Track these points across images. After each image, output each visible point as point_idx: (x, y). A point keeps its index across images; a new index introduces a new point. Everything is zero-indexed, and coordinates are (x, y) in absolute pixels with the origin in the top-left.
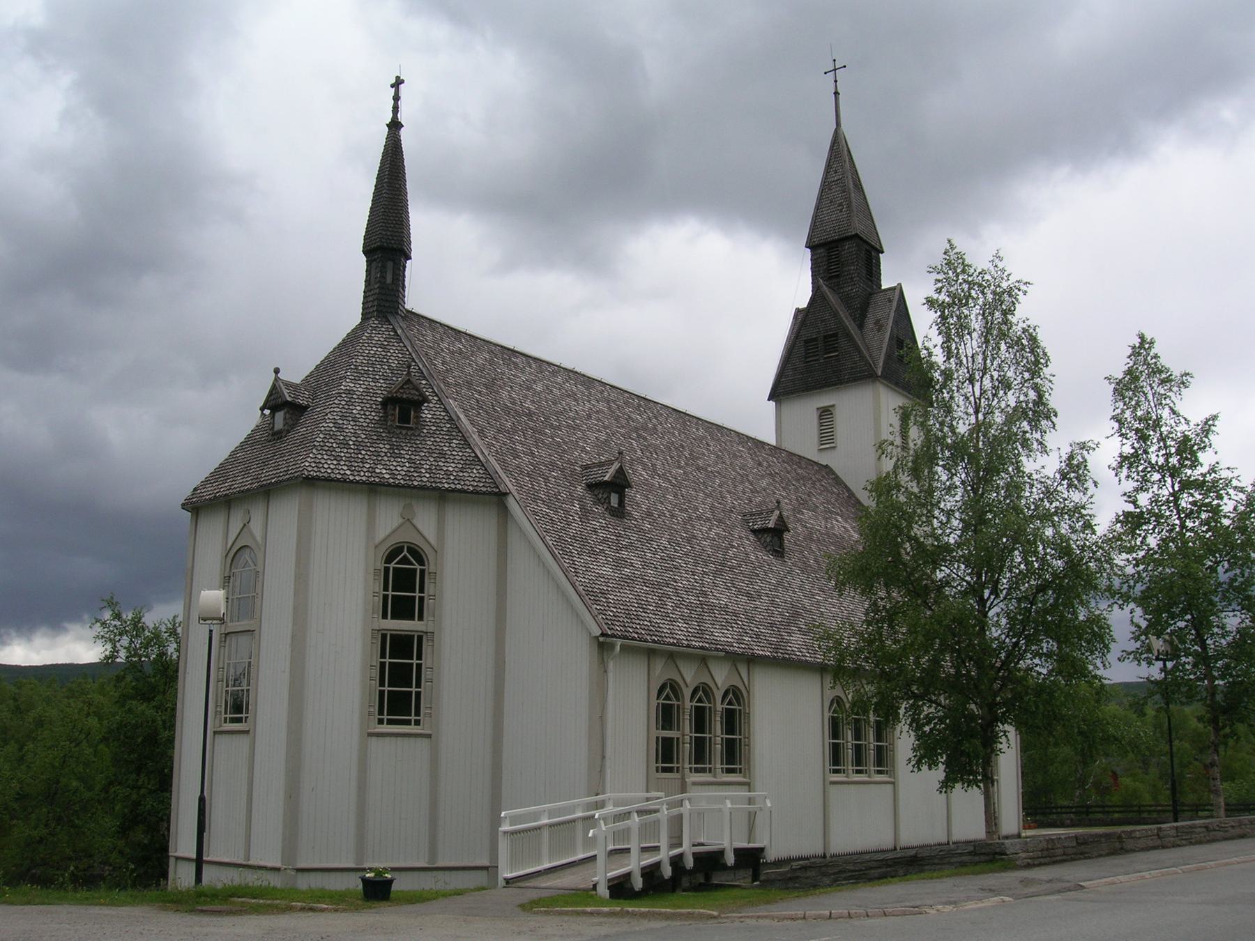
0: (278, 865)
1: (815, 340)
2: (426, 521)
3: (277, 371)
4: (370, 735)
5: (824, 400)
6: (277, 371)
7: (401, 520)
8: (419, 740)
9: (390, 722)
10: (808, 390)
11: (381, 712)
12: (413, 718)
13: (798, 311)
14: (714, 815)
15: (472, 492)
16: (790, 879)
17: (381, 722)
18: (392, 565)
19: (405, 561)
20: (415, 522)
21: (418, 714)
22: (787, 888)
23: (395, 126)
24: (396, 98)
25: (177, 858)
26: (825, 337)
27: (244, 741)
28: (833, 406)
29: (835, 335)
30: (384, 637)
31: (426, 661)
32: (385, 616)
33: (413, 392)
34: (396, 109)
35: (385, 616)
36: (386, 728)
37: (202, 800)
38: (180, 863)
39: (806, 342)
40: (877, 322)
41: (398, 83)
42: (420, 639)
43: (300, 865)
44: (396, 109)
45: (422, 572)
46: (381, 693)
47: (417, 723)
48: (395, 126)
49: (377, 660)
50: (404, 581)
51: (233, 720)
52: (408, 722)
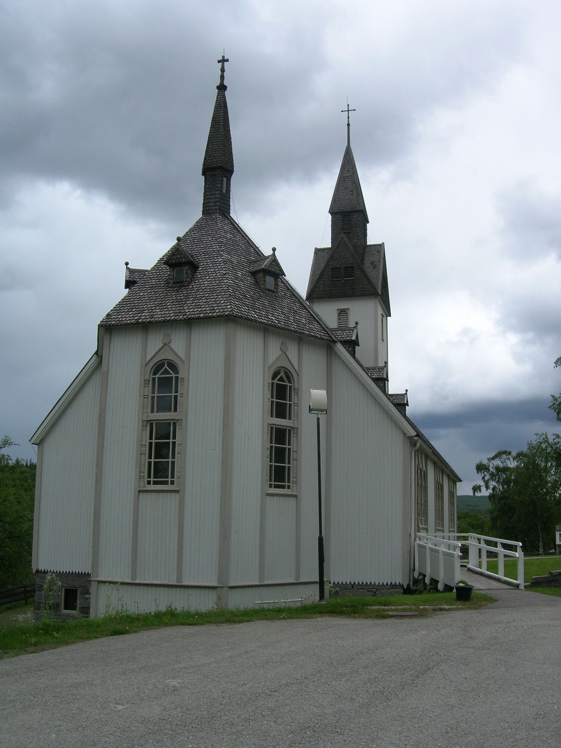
0: (215, 584)
1: (339, 268)
2: (178, 343)
3: (127, 264)
4: (268, 495)
5: (343, 305)
6: (127, 264)
7: (280, 352)
8: (169, 495)
9: (155, 483)
10: (333, 298)
11: (149, 477)
12: (169, 479)
13: (318, 252)
14: (464, 542)
15: (319, 339)
16: (552, 581)
17: (149, 483)
18: (275, 381)
19: (281, 379)
20: (287, 353)
21: (173, 477)
22: (550, 586)
23: (222, 88)
24: (223, 70)
25: (99, 582)
26: (346, 268)
27: (173, 499)
28: (348, 309)
29: (352, 267)
30: (272, 428)
31: (293, 447)
32: (152, 412)
33: (277, 268)
34: (222, 77)
35: (152, 412)
36: (152, 487)
37: (321, 540)
38: (103, 587)
39: (332, 269)
40: (372, 263)
41: (223, 61)
42: (290, 431)
43: (99, 579)
44: (222, 77)
45: (177, 378)
46: (271, 466)
47: (289, 487)
48: (222, 88)
49: (146, 441)
50: (282, 391)
51: (276, 486)
52: (166, 483)
